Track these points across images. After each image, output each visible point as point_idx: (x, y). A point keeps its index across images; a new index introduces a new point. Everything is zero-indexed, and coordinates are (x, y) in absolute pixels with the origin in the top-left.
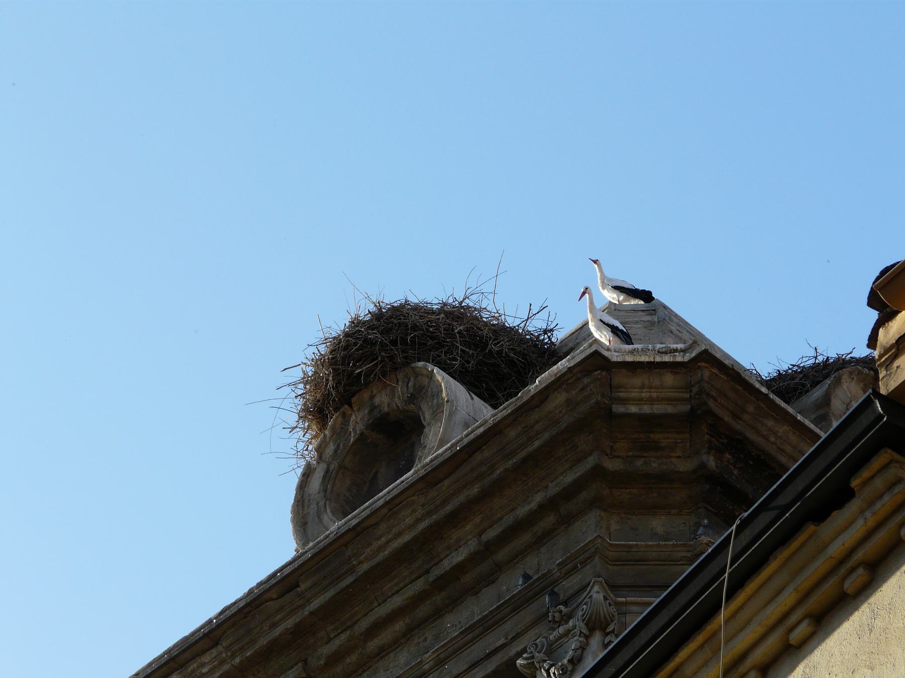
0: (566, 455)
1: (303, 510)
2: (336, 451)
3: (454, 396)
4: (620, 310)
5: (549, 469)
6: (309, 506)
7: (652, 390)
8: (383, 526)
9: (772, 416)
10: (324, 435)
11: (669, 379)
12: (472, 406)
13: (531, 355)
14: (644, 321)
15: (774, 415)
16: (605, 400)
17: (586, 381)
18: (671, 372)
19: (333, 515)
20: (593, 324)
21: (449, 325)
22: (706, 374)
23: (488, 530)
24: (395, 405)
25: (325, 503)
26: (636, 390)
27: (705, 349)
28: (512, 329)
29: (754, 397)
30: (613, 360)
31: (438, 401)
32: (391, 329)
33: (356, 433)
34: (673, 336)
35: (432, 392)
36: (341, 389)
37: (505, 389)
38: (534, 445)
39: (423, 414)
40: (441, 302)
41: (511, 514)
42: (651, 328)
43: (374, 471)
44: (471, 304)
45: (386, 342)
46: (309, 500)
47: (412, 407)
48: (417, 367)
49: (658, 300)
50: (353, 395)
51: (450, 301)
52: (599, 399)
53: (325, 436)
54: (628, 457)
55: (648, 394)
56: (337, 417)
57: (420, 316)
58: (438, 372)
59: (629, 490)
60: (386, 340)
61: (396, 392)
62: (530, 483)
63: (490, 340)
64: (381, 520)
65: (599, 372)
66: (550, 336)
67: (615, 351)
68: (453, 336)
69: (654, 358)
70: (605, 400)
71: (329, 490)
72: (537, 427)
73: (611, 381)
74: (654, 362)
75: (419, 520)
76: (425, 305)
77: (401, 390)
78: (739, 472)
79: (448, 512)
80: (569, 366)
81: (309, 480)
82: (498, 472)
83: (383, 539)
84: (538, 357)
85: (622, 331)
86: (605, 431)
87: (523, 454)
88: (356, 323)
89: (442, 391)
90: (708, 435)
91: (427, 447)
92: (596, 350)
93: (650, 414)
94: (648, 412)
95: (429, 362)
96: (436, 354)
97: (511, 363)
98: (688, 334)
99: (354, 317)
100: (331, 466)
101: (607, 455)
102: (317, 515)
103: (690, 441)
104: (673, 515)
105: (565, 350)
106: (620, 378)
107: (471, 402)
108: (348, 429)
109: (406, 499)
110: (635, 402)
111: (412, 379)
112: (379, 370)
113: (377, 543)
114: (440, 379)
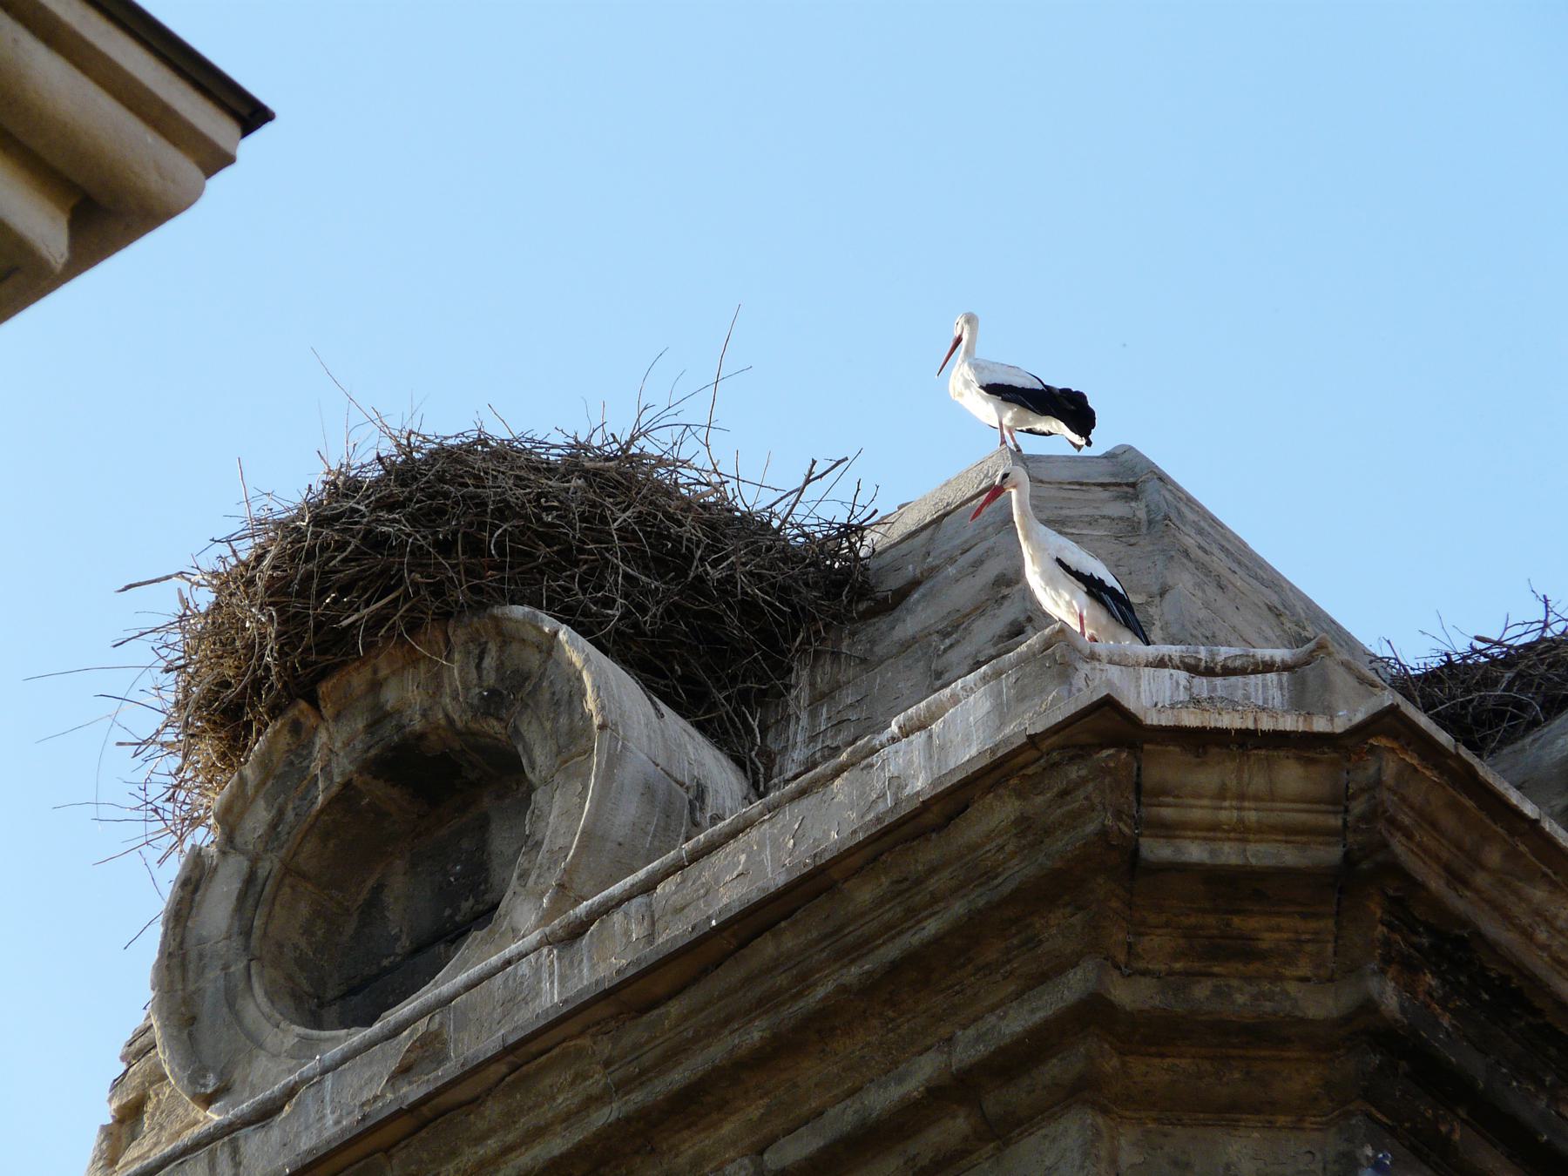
0: (1009, 961)
1: (184, 979)
2: (274, 826)
4: (1041, 482)
5: (957, 993)
6: (201, 972)
7: (1246, 804)
8: (493, 1110)
9: (1545, 875)
10: (241, 777)
11: (1291, 776)
12: (659, 737)
13: (804, 590)
14: (1109, 518)
15: (1549, 872)
16: (1121, 825)
17: (1074, 772)
18: (1299, 758)
19: (272, 1002)
20: (1036, 569)
21: (593, 505)
22: (1390, 768)
23: (782, 1141)
24: (441, 716)
25: (248, 968)
26: (1205, 802)
27: (1392, 704)
28: (747, 518)
29: (1502, 827)
30: (1148, 722)
31: (572, 720)
32: (441, 512)
33: (331, 780)
35: (554, 694)
36: (295, 659)
37: (733, 679)
38: (924, 929)
39: (529, 751)
41: (848, 1102)
43: (371, 883)
44: (651, 449)
45: (423, 543)
46: (201, 956)
47: (493, 726)
48: (510, 619)
49: (1138, 454)
50: (324, 674)
51: (596, 441)
52: (1109, 822)
53: (242, 780)
54: (1171, 973)
55: (1235, 813)
56: (276, 733)
57: (517, 477)
58: (572, 643)
59: (1169, 1060)
60: (425, 538)
61: (446, 681)
62: (906, 1026)
64: (489, 1092)
65: (1111, 751)
66: (856, 542)
68: (603, 537)
69: (1255, 720)
70: (1121, 825)
71: (257, 933)
72: (933, 884)
73: (1138, 775)
74: (1256, 730)
75: (592, 1102)
77: (460, 674)
78: (1454, 1022)
79: (676, 1087)
81: (197, 897)
82: (821, 992)
83: (492, 1144)
85: (1112, 591)
86: (1114, 904)
87: (891, 951)
88: (344, 487)
89: (584, 695)
90: (1383, 924)
92: (1108, 695)
93: (1238, 866)
95: (540, 607)
96: (559, 586)
97: (749, 608)
98: (1222, 556)
99: (335, 467)
100: (260, 865)
101: (1120, 969)
102: (227, 1000)
103: (1336, 939)
104: (1280, 1129)
105: (893, 582)
106: (1165, 769)
108: (309, 767)
109: (558, 1044)
110: (1199, 834)
111: (492, 647)
113: (476, 1153)
114: (577, 659)
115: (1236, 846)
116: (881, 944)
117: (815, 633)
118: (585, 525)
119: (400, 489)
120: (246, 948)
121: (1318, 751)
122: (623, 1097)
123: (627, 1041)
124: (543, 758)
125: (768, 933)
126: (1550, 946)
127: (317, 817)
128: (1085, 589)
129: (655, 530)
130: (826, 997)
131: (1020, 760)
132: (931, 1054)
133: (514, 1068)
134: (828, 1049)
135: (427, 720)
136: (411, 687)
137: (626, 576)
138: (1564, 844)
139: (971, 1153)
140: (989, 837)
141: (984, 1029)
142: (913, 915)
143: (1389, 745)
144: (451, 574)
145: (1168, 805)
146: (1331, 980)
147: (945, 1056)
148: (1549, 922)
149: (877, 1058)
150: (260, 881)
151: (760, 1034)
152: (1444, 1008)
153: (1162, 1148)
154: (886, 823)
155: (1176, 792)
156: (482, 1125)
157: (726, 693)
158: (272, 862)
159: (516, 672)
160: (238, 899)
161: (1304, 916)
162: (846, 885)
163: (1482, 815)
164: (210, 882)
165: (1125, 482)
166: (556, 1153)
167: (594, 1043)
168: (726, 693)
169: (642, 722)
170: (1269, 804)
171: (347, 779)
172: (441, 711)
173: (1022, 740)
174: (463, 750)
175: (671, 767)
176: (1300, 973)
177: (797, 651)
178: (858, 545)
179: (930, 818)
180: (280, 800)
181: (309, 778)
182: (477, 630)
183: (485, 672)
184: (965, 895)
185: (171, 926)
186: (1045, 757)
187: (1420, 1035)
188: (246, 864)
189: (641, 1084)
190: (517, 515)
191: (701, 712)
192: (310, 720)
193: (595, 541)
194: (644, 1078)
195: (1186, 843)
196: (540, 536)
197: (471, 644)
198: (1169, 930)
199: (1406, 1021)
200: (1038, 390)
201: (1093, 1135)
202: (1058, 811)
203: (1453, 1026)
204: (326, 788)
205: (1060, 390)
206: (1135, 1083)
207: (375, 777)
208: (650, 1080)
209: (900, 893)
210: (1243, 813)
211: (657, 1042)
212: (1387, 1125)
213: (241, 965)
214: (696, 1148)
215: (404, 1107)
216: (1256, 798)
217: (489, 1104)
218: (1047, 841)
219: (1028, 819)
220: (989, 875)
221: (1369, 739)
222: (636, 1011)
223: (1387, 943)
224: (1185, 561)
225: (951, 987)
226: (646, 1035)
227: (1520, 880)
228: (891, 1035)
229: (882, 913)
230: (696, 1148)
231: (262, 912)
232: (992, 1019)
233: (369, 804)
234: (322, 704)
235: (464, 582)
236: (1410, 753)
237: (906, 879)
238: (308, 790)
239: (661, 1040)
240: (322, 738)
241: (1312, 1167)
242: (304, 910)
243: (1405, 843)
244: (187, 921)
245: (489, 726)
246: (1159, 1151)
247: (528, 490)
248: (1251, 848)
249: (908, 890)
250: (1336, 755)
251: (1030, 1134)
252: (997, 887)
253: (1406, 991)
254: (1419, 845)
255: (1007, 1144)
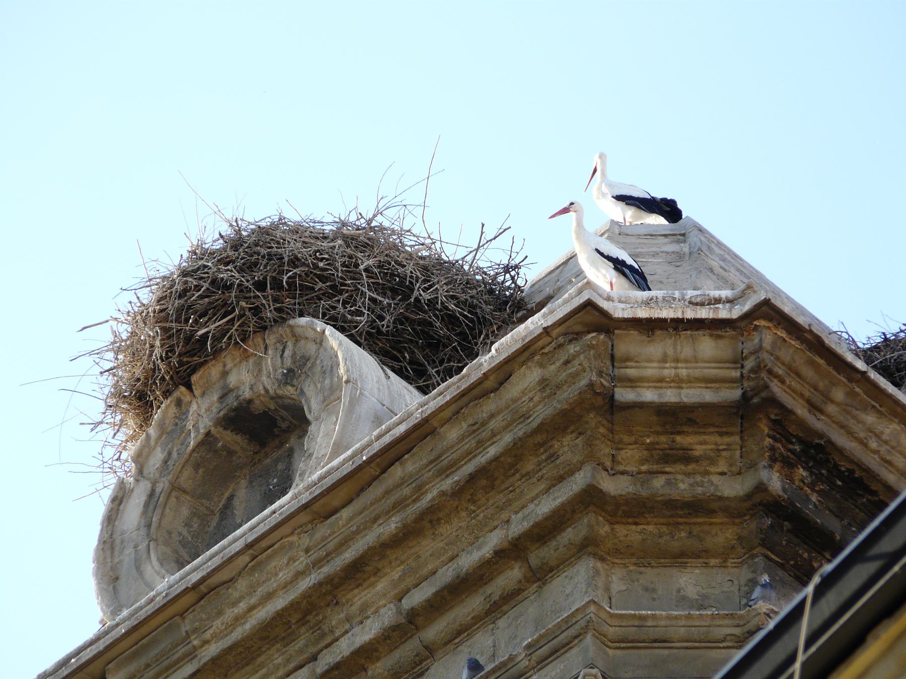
0: (540, 470)
2: (165, 462)
3: (358, 373)
4: (627, 235)
5: (511, 492)
7: (680, 365)
8: (242, 584)
9: (874, 407)
11: (707, 346)
14: (666, 252)
15: (877, 405)
16: (602, 380)
17: (572, 349)
18: (711, 335)
21: (350, 257)
22: (768, 339)
24: (261, 388)
25: (149, 546)
26: (655, 365)
27: (765, 298)
28: (453, 264)
29: (843, 377)
30: (616, 316)
32: (256, 264)
34: (714, 277)
40: (337, 220)
41: (450, 564)
42: (678, 264)
43: (227, 495)
46: (122, 542)
47: (289, 391)
48: (299, 326)
50: (194, 370)
51: (353, 218)
52: (594, 378)
53: (148, 437)
54: (639, 473)
55: (673, 371)
56: (167, 407)
57: (304, 242)
58: (332, 335)
59: (640, 526)
62: (482, 515)
63: (417, 281)
65: (594, 334)
67: (620, 301)
68: (356, 277)
70: (602, 380)
71: (154, 525)
73: (612, 350)
74: (683, 319)
76: (312, 224)
80: (546, 326)
81: (122, 507)
82: (429, 496)
83: (243, 606)
84: (495, 311)
85: (631, 268)
86: (602, 430)
87: (469, 468)
88: (199, 254)
89: (339, 365)
90: (769, 437)
91: (314, 457)
92: (589, 299)
94: (673, 399)
97: (451, 320)
98: (738, 274)
99: (195, 243)
102: (135, 565)
103: (741, 448)
104: (713, 567)
105: (538, 299)
107: (385, 383)
108: (185, 425)
110: (651, 384)
112: (237, 330)
115: (675, 391)
116: (464, 465)
117: (492, 333)
118: (345, 268)
119: (233, 253)
120: (148, 535)
121: (723, 330)
122: (317, 571)
123: (318, 536)
124: (315, 405)
125: (397, 463)
126: (879, 451)
127: (190, 455)
128: (613, 266)
129: (390, 271)
130: (433, 499)
131: (540, 343)
132: (497, 531)
133: (254, 558)
134: (437, 532)
135: (253, 391)
136: (244, 372)
137: (372, 300)
138: (884, 387)
139: (524, 590)
140: (523, 393)
141: (527, 513)
142: (481, 445)
143: (767, 325)
144: (264, 302)
145: (632, 367)
146: (739, 473)
147: (505, 531)
148: (878, 436)
149: (465, 536)
150: (157, 494)
151: (395, 525)
152: (813, 490)
153: (638, 581)
154: (462, 388)
155: (636, 359)
156: (236, 595)
157: (435, 370)
158: (164, 483)
159: (303, 357)
160: (144, 506)
161: (721, 434)
162: (442, 429)
163: (831, 369)
164: (129, 498)
165: (679, 233)
166: (279, 607)
167: (299, 538)
168: (435, 370)
169: (375, 380)
170: (694, 365)
171: (207, 431)
172: (261, 385)
173: (540, 330)
174: (276, 409)
175: (393, 407)
176: (720, 470)
177: (481, 343)
178: (516, 278)
179: (489, 384)
180: (169, 446)
181: (186, 431)
182: (281, 335)
183: (285, 359)
184: (512, 430)
185: (105, 525)
186: (555, 341)
187: (796, 505)
188: (149, 485)
189: (328, 561)
190: (304, 264)
191: (422, 381)
192: (187, 397)
193: (351, 279)
194: (329, 558)
195: (644, 390)
196: (318, 276)
197: (278, 344)
198: (638, 445)
199: (786, 496)
200: (647, 199)
201: (594, 573)
202: (564, 374)
203: (819, 501)
204: (196, 437)
205: (661, 199)
206: (620, 541)
207: (225, 429)
208: (332, 559)
209: (474, 431)
210: (678, 370)
211: (334, 536)
212: (779, 562)
213: (145, 544)
214: (363, 600)
215: (189, 586)
216: (686, 361)
217: (240, 581)
218: (558, 393)
219: (547, 379)
220: (525, 417)
221: (755, 320)
222: (324, 518)
223: (772, 449)
224: (710, 274)
225: (507, 488)
226: (329, 531)
227: (857, 409)
228: (473, 521)
229: (464, 445)
230: (363, 600)
231: (158, 512)
232: (531, 506)
233: (223, 446)
234: (194, 387)
235: (271, 305)
236: (780, 329)
237: (476, 423)
238: (185, 439)
239: (338, 533)
240: (194, 407)
241: (732, 589)
242: (185, 512)
243: (780, 386)
244: (115, 522)
245: (287, 391)
246: (636, 582)
247: (309, 249)
248: (684, 392)
249: (478, 429)
250: (734, 333)
251: (558, 577)
252: (530, 423)
253: (787, 479)
254: (789, 387)
255: (544, 584)
